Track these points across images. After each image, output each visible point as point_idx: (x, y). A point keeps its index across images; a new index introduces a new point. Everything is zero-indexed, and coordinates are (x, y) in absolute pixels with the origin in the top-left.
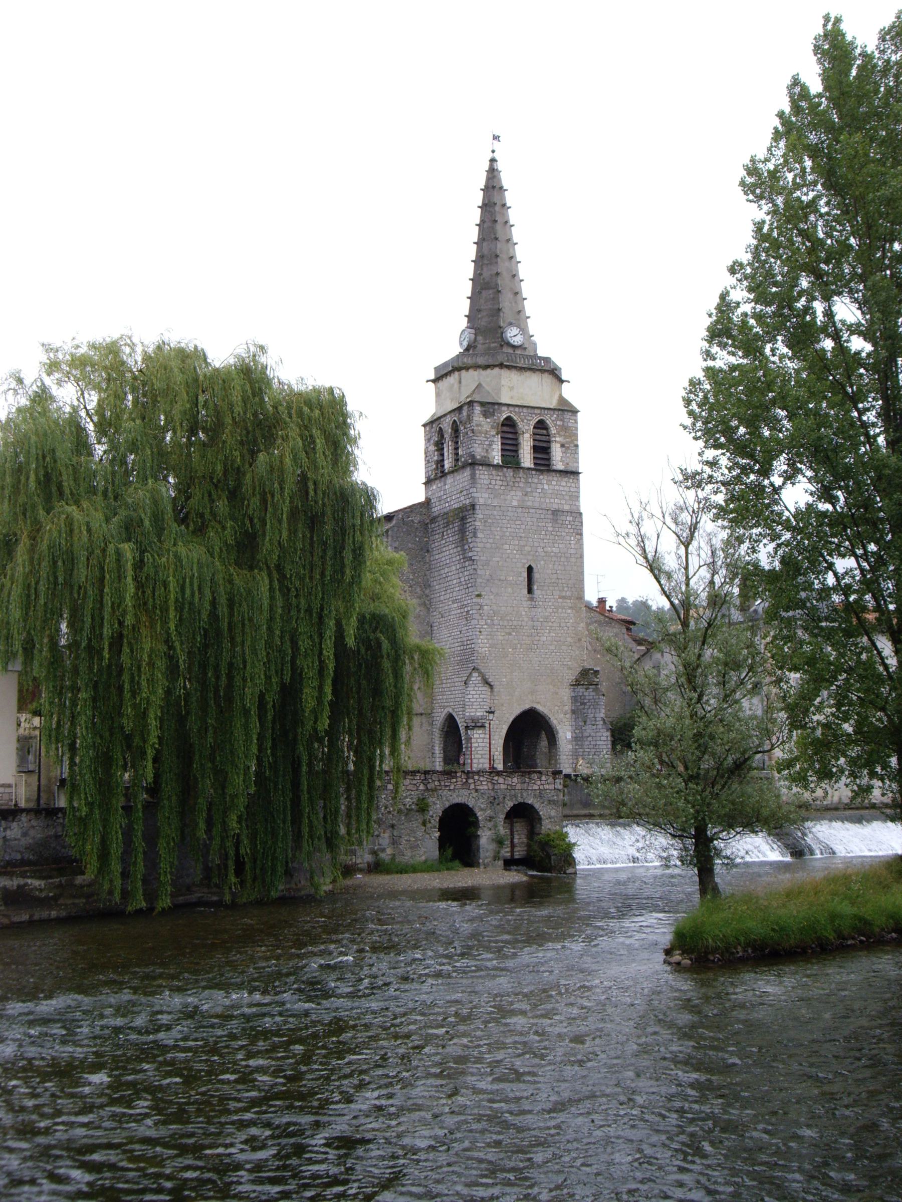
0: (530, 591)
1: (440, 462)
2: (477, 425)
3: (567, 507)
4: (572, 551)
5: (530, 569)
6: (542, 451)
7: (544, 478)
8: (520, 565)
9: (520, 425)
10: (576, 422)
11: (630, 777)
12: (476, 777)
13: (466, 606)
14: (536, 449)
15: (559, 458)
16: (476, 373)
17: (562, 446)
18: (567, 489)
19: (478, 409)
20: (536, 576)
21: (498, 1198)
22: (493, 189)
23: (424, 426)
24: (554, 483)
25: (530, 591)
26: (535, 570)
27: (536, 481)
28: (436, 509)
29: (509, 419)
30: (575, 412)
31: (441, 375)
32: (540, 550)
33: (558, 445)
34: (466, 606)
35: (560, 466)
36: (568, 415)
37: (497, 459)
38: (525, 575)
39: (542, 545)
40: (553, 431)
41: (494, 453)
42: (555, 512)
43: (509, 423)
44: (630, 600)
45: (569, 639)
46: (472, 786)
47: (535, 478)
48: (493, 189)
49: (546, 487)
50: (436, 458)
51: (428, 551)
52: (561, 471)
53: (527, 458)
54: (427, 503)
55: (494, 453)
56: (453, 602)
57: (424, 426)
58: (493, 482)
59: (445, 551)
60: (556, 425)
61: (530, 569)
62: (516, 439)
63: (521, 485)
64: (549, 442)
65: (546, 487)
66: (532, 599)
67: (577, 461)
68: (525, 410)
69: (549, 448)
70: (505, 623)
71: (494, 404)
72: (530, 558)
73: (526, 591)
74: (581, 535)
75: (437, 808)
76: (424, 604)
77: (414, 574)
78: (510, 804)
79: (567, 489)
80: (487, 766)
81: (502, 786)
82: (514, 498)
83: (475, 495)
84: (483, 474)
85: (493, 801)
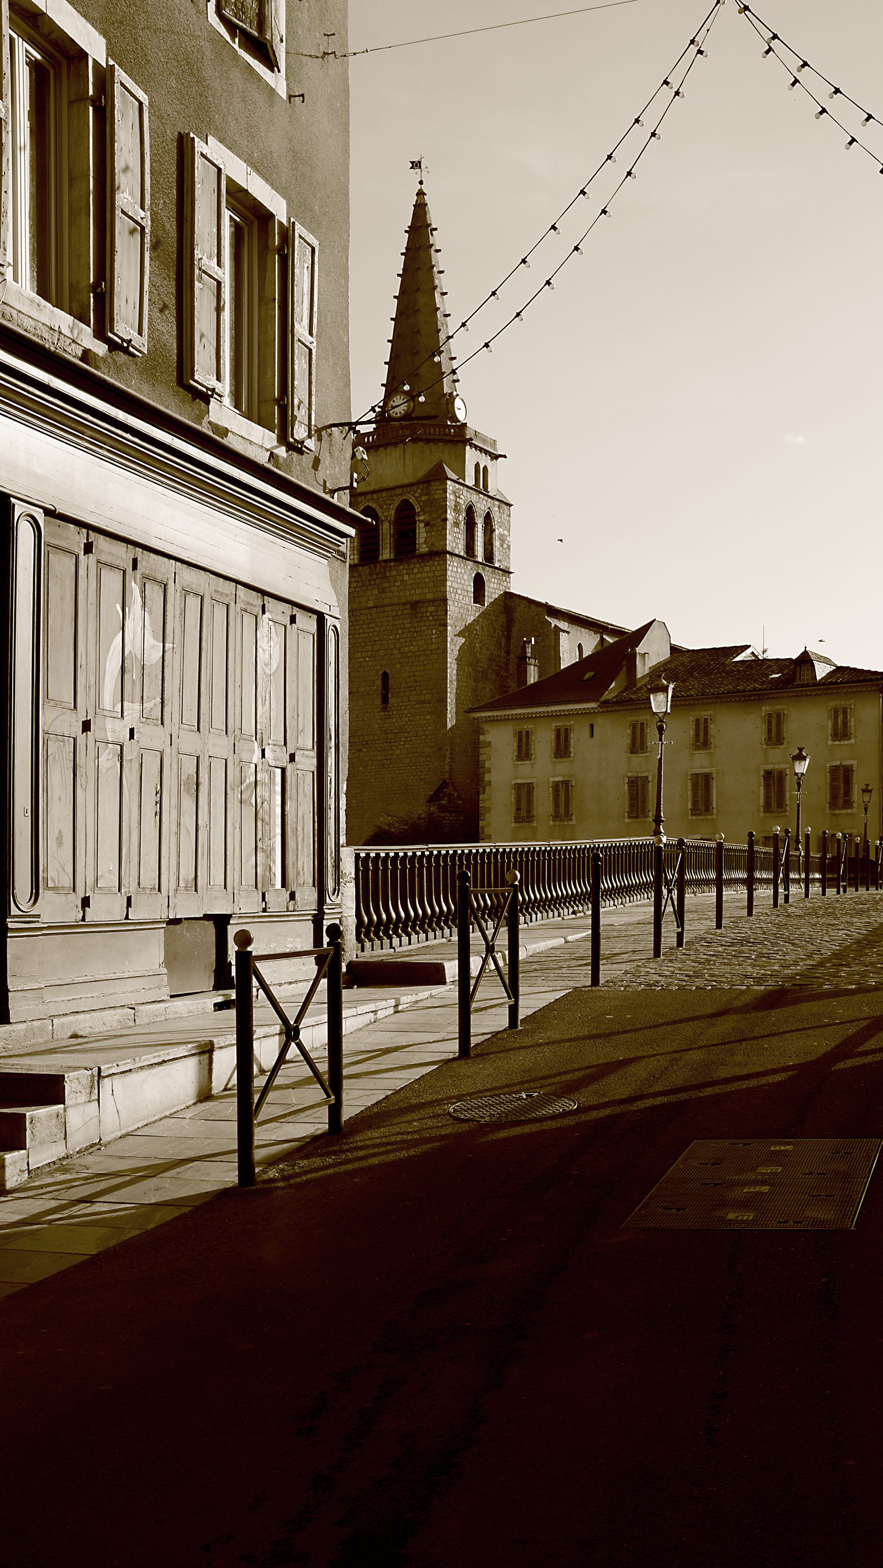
0: (385, 699)
3: (430, 596)
5: (385, 676)
15: (422, 540)
17: (427, 524)
22: (420, 209)
25: (385, 699)
32: (396, 652)
38: (379, 683)
42: (415, 605)
45: (427, 750)
48: (420, 209)
61: (385, 676)
65: (406, 577)
68: (384, 494)
73: (378, 701)
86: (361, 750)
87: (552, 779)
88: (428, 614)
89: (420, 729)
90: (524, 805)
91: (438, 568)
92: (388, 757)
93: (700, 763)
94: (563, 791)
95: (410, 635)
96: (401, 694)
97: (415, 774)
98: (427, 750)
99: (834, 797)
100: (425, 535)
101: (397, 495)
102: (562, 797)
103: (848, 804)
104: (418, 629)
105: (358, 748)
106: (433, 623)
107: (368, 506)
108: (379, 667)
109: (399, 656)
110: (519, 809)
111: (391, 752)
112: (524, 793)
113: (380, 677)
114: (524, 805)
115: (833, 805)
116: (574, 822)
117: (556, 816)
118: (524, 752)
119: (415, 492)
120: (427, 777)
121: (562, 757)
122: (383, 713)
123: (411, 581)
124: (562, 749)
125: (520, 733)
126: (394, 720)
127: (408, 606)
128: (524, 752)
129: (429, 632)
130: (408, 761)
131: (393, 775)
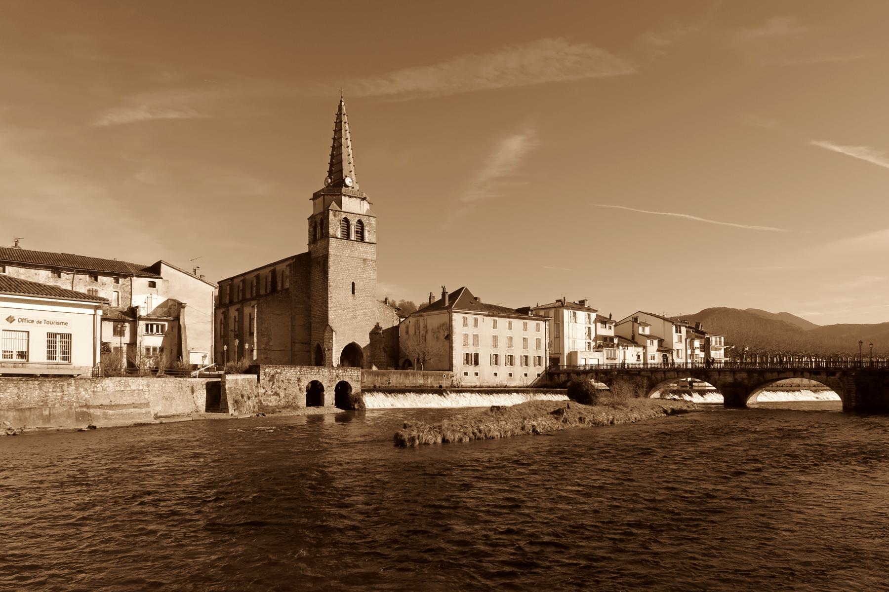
0: (353, 293)
1: (315, 235)
5: (353, 284)
7: (360, 244)
11: (647, 452)
21: (821, 575)
25: (353, 293)
28: (313, 256)
29: (345, 218)
31: (316, 196)
37: (339, 235)
42: (365, 260)
43: (346, 220)
44: (406, 301)
47: (356, 244)
53: (353, 236)
54: (308, 254)
61: (353, 284)
75: (305, 383)
78: (338, 381)
80: (7, 267)
82: (347, 253)
85: (331, 380)
93: (510, 334)
94: (476, 337)
112: (465, 336)
118: (465, 324)
128: (465, 324)
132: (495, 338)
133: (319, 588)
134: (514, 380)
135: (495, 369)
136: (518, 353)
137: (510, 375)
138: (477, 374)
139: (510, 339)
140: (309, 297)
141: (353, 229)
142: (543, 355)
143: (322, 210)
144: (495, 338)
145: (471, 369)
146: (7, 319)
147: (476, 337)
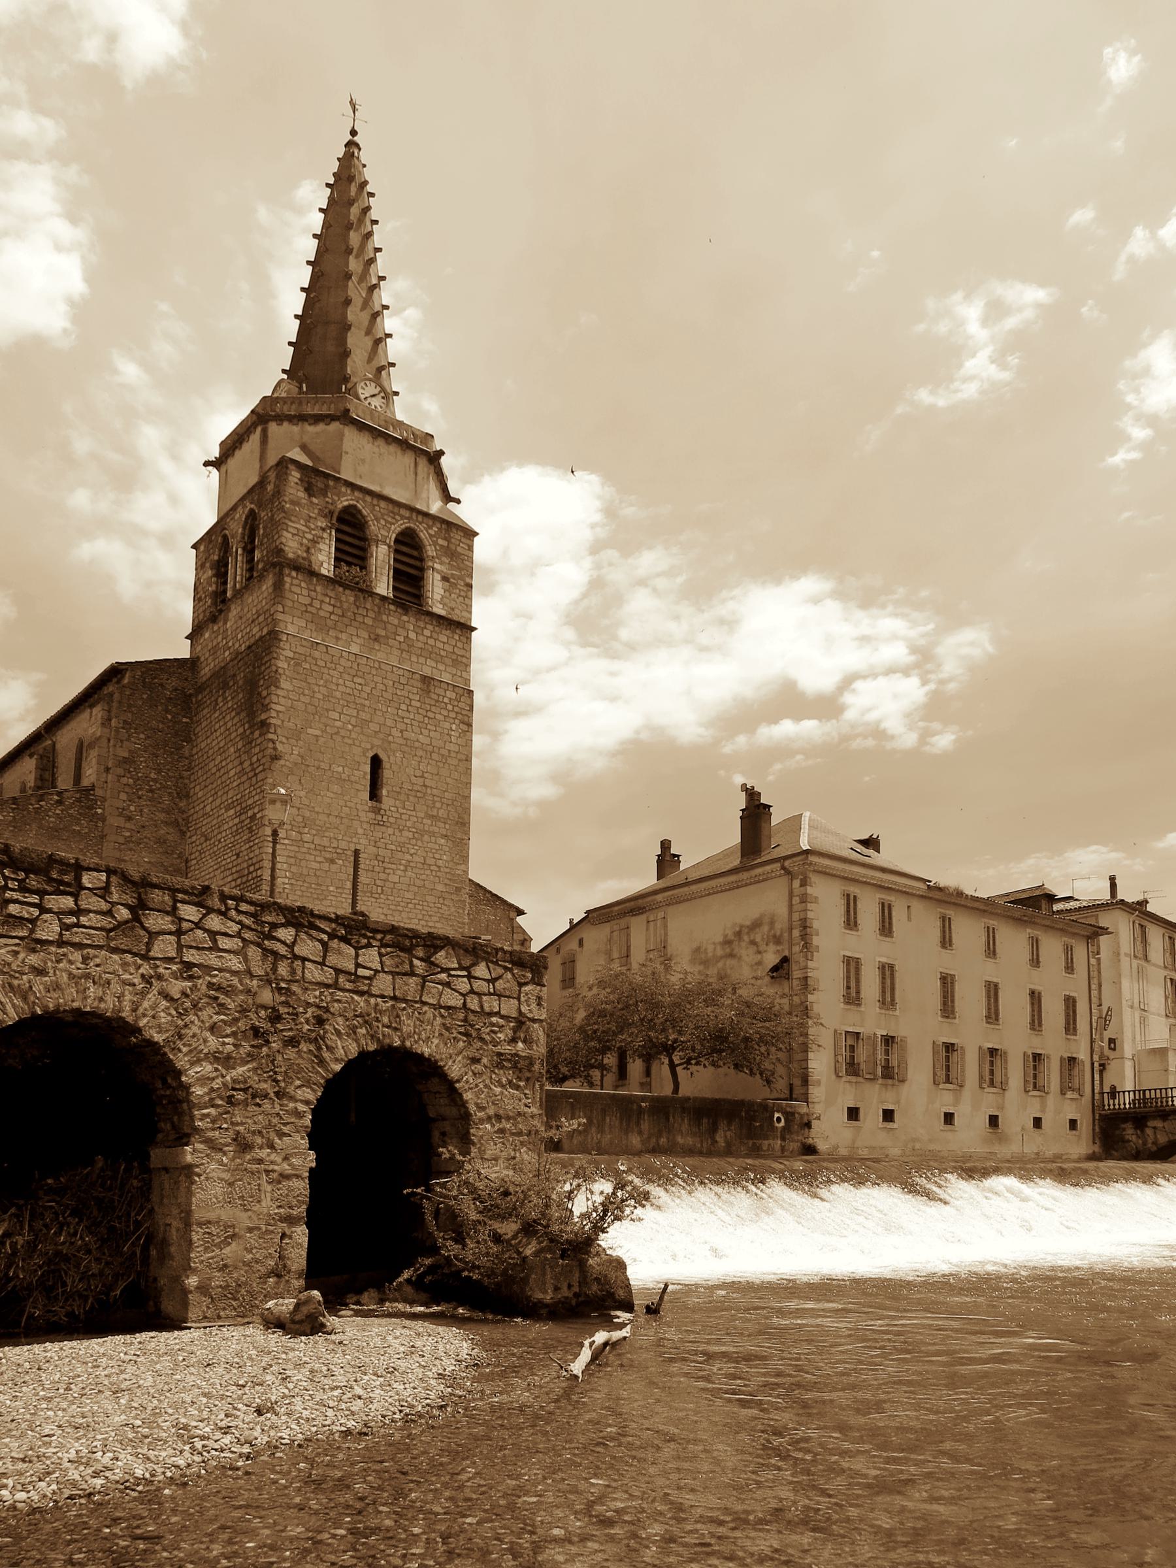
0: (374, 795)
2: (292, 503)
4: (453, 747)
5: (376, 763)
6: (410, 581)
7: (409, 620)
8: (357, 751)
9: (374, 528)
10: (471, 548)
12: (189, 912)
13: (250, 807)
14: (398, 575)
15: (437, 597)
16: (296, 429)
17: (445, 579)
18: (448, 648)
19: (295, 475)
20: (387, 774)
23: (194, 546)
24: (427, 633)
26: (386, 765)
27: (396, 622)
30: (471, 534)
32: (395, 732)
33: (438, 577)
34: (250, 807)
35: (438, 610)
36: (456, 535)
38: (368, 768)
39: (401, 726)
40: (430, 551)
41: (322, 557)
42: (426, 680)
45: (440, 887)
46: (165, 947)
47: (393, 618)
49: (412, 635)
50: (213, 588)
51: (189, 741)
52: (440, 617)
54: (190, 665)
55: (322, 557)
56: (227, 809)
57: (194, 546)
58: (317, 604)
59: (218, 730)
60: (435, 544)
62: (364, 550)
63: (369, 621)
64: (422, 570)
65: (412, 635)
66: (377, 811)
67: (468, 608)
68: (383, 504)
69: (421, 579)
70: (326, 842)
71: (327, 476)
72: (377, 742)
73: (366, 795)
74: (470, 725)
76: (176, 824)
77: (159, 772)
79: (448, 648)
81: (313, 973)
83: (280, 616)
84: (296, 587)
86: (332, 861)
87: (878, 959)
88: (446, 700)
89: (430, 855)
90: (853, 985)
91: (459, 644)
92: (379, 882)
93: (990, 971)
94: (887, 972)
95: (420, 718)
96: (403, 797)
97: (420, 917)
98: (440, 887)
99: (1032, 1022)
100: (442, 592)
101: (403, 517)
102: (888, 981)
103: (1075, 1032)
104: (430, 714)
105: (328, 856)
106: (453, 715)
107: (355, 506)
108: (369, 746)
109: (402, 741)
110: (848, 988)
111: (382, 876)
112: (852, 966)
113: (369, 762)
114: (853, 985)
115: (1067, 1030)
116: (897, 1013)
117: (883, 1003)
119: (430, 527)
120: (438, 925)
121: (886, 936)
122: (372, 815)
123: (420, 645)
124: (886, 928)
125: (848, 895)
126: (390, 831)
127: (417, 677)
128: (851, 922)
129: (447, 725)
130: (407, 895)
131: (385, 911)
132: (947, 982)
133: (941, 403)
134: (1002, 1139)
135: (945, 1101)
136: (1015, 1038)
137: (994, 1121)
138: (888, 1115)
139: (992, 990)
140: (182, 826)
141: (381, 557)
142: (1083, 1055)
143: (254, 480)
144: (947, 982)
145: (873, 1099)
146: (885, 1111)
147: (887, 972)
